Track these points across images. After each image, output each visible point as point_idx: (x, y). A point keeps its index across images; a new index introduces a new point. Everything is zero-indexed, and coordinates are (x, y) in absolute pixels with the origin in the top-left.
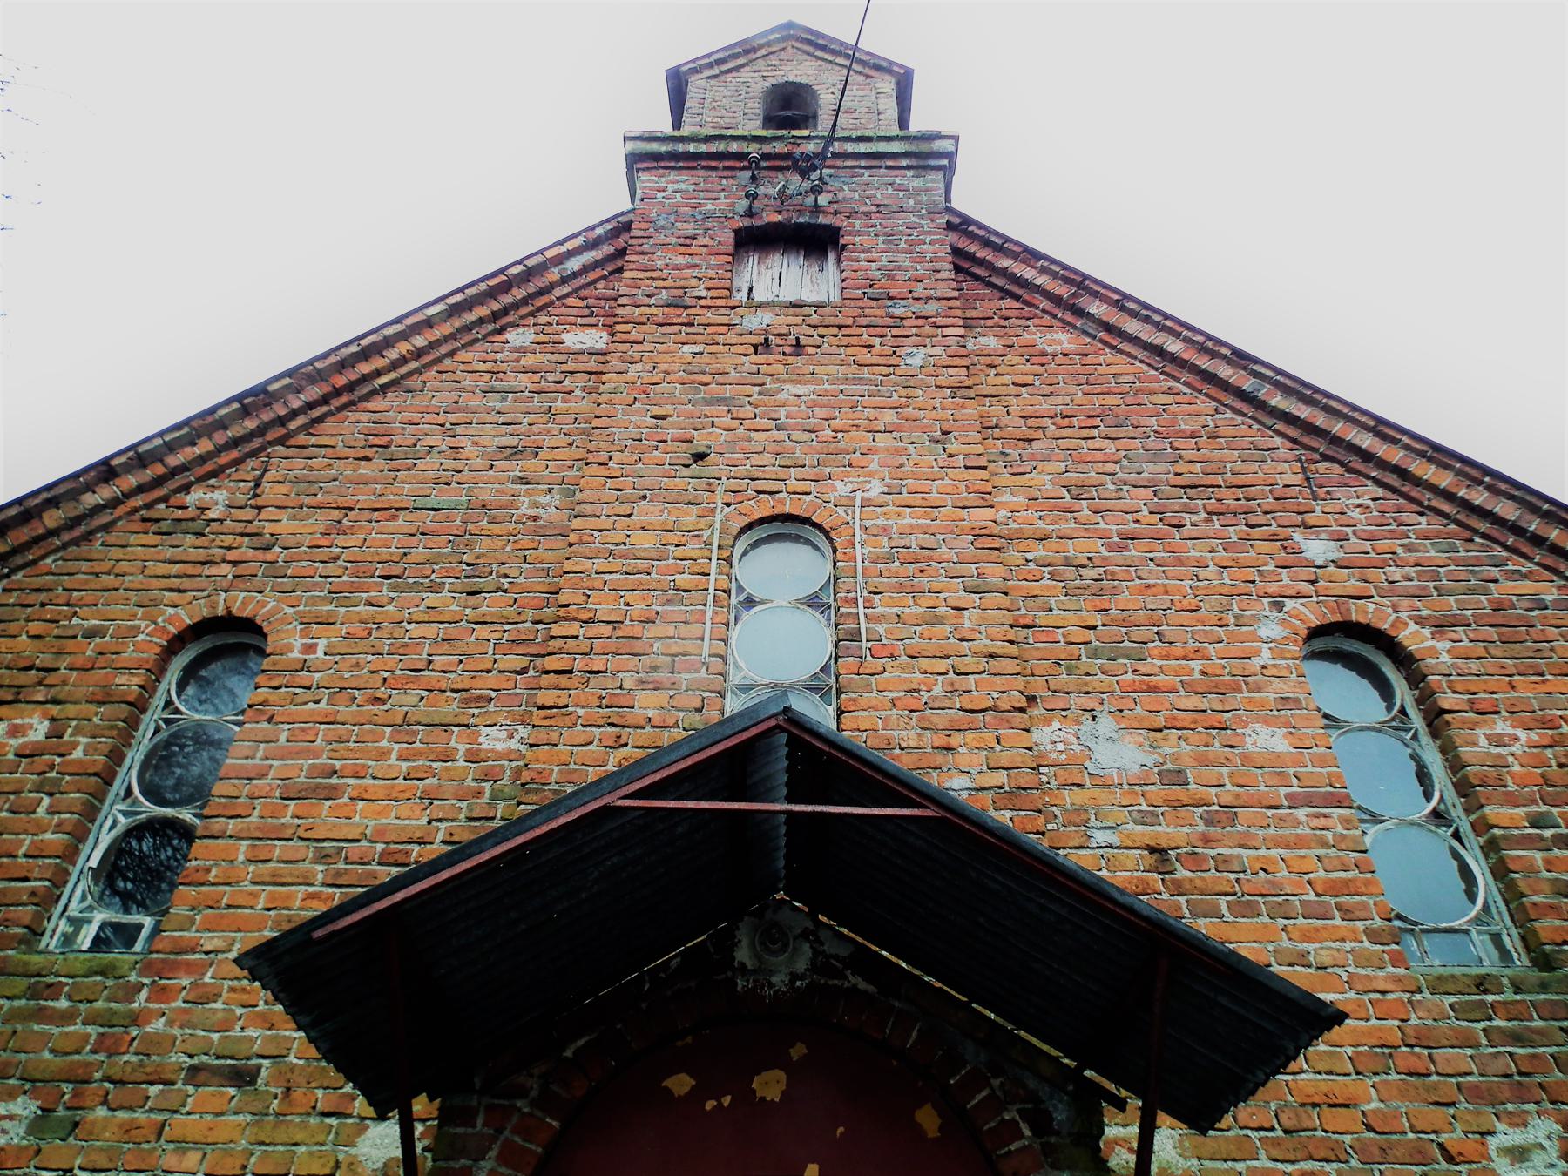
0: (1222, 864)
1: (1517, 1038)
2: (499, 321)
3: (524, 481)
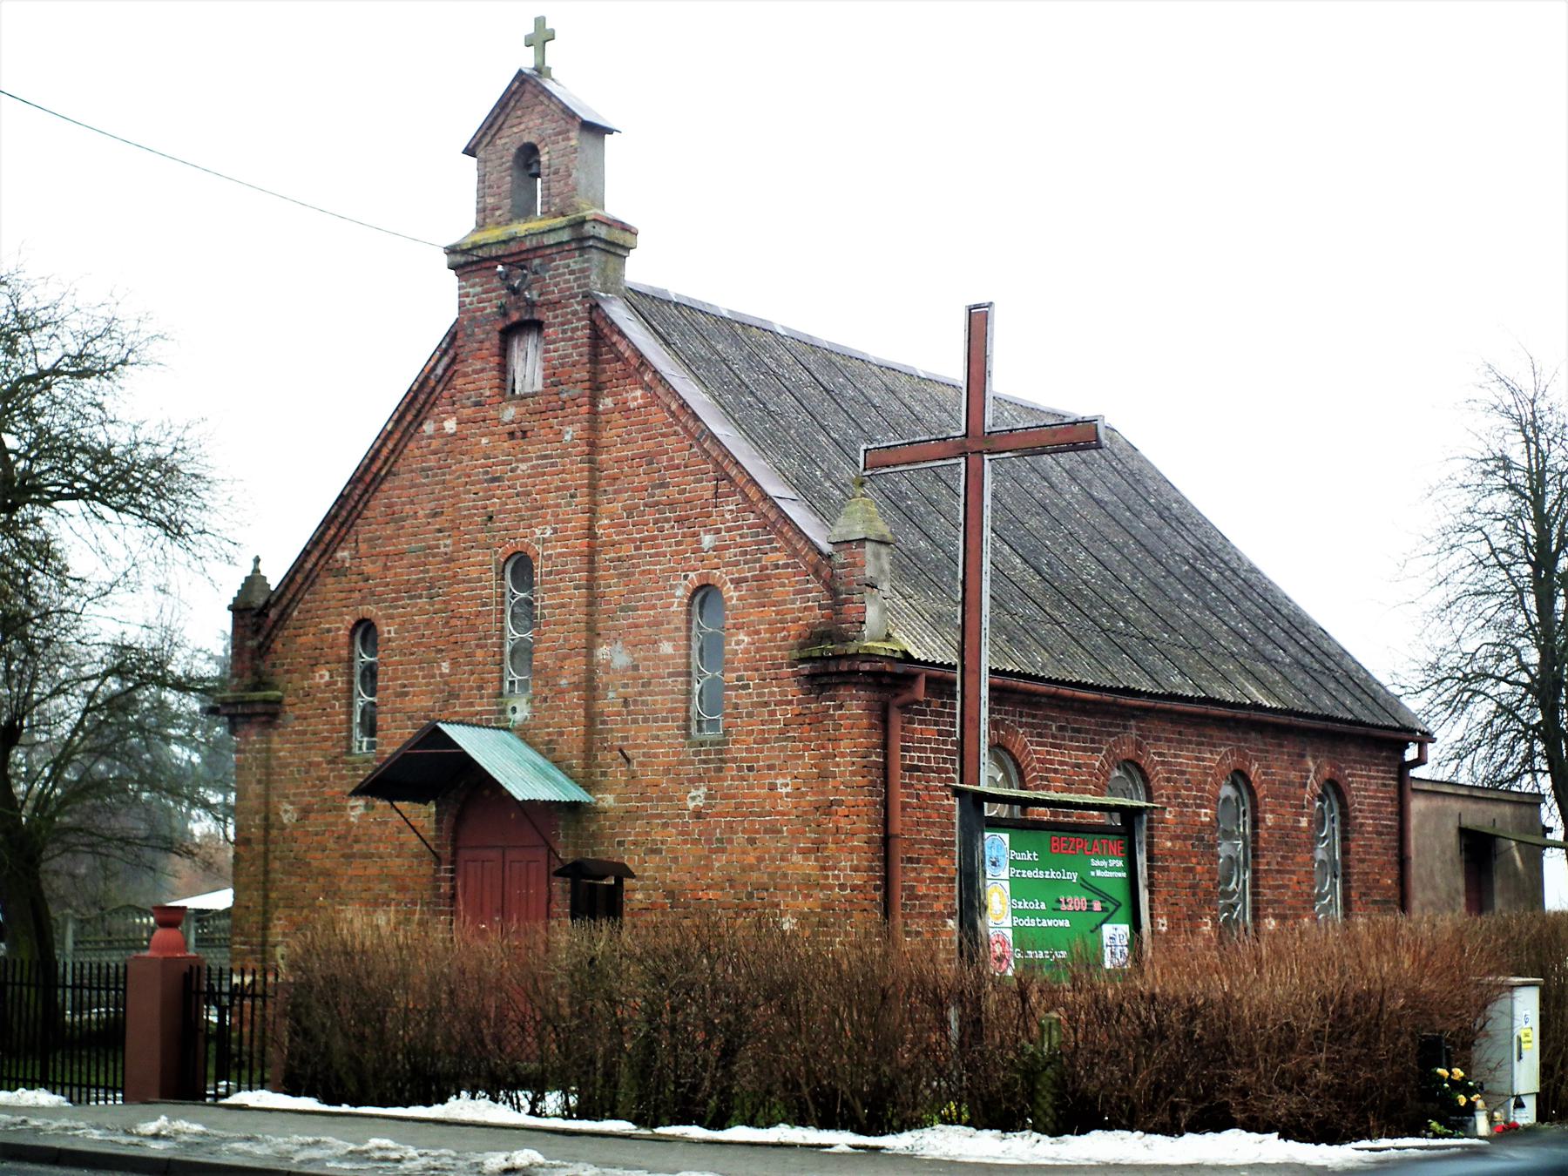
0: (644, 703)
1: (705, 762)
2: (419, 421)
3: (440, 531)
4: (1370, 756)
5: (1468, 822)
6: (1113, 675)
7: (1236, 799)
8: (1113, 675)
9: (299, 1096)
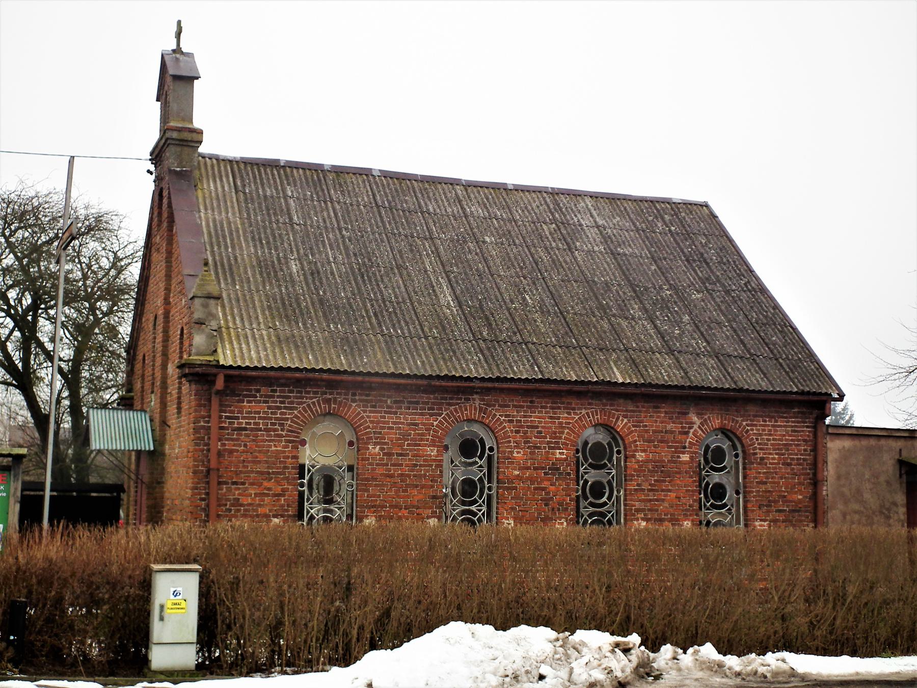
4: (776, 412)
5: (905, 455)
6: (686, 373)
7: (609, 444)
8: (686, 373)
9: (509, 629)
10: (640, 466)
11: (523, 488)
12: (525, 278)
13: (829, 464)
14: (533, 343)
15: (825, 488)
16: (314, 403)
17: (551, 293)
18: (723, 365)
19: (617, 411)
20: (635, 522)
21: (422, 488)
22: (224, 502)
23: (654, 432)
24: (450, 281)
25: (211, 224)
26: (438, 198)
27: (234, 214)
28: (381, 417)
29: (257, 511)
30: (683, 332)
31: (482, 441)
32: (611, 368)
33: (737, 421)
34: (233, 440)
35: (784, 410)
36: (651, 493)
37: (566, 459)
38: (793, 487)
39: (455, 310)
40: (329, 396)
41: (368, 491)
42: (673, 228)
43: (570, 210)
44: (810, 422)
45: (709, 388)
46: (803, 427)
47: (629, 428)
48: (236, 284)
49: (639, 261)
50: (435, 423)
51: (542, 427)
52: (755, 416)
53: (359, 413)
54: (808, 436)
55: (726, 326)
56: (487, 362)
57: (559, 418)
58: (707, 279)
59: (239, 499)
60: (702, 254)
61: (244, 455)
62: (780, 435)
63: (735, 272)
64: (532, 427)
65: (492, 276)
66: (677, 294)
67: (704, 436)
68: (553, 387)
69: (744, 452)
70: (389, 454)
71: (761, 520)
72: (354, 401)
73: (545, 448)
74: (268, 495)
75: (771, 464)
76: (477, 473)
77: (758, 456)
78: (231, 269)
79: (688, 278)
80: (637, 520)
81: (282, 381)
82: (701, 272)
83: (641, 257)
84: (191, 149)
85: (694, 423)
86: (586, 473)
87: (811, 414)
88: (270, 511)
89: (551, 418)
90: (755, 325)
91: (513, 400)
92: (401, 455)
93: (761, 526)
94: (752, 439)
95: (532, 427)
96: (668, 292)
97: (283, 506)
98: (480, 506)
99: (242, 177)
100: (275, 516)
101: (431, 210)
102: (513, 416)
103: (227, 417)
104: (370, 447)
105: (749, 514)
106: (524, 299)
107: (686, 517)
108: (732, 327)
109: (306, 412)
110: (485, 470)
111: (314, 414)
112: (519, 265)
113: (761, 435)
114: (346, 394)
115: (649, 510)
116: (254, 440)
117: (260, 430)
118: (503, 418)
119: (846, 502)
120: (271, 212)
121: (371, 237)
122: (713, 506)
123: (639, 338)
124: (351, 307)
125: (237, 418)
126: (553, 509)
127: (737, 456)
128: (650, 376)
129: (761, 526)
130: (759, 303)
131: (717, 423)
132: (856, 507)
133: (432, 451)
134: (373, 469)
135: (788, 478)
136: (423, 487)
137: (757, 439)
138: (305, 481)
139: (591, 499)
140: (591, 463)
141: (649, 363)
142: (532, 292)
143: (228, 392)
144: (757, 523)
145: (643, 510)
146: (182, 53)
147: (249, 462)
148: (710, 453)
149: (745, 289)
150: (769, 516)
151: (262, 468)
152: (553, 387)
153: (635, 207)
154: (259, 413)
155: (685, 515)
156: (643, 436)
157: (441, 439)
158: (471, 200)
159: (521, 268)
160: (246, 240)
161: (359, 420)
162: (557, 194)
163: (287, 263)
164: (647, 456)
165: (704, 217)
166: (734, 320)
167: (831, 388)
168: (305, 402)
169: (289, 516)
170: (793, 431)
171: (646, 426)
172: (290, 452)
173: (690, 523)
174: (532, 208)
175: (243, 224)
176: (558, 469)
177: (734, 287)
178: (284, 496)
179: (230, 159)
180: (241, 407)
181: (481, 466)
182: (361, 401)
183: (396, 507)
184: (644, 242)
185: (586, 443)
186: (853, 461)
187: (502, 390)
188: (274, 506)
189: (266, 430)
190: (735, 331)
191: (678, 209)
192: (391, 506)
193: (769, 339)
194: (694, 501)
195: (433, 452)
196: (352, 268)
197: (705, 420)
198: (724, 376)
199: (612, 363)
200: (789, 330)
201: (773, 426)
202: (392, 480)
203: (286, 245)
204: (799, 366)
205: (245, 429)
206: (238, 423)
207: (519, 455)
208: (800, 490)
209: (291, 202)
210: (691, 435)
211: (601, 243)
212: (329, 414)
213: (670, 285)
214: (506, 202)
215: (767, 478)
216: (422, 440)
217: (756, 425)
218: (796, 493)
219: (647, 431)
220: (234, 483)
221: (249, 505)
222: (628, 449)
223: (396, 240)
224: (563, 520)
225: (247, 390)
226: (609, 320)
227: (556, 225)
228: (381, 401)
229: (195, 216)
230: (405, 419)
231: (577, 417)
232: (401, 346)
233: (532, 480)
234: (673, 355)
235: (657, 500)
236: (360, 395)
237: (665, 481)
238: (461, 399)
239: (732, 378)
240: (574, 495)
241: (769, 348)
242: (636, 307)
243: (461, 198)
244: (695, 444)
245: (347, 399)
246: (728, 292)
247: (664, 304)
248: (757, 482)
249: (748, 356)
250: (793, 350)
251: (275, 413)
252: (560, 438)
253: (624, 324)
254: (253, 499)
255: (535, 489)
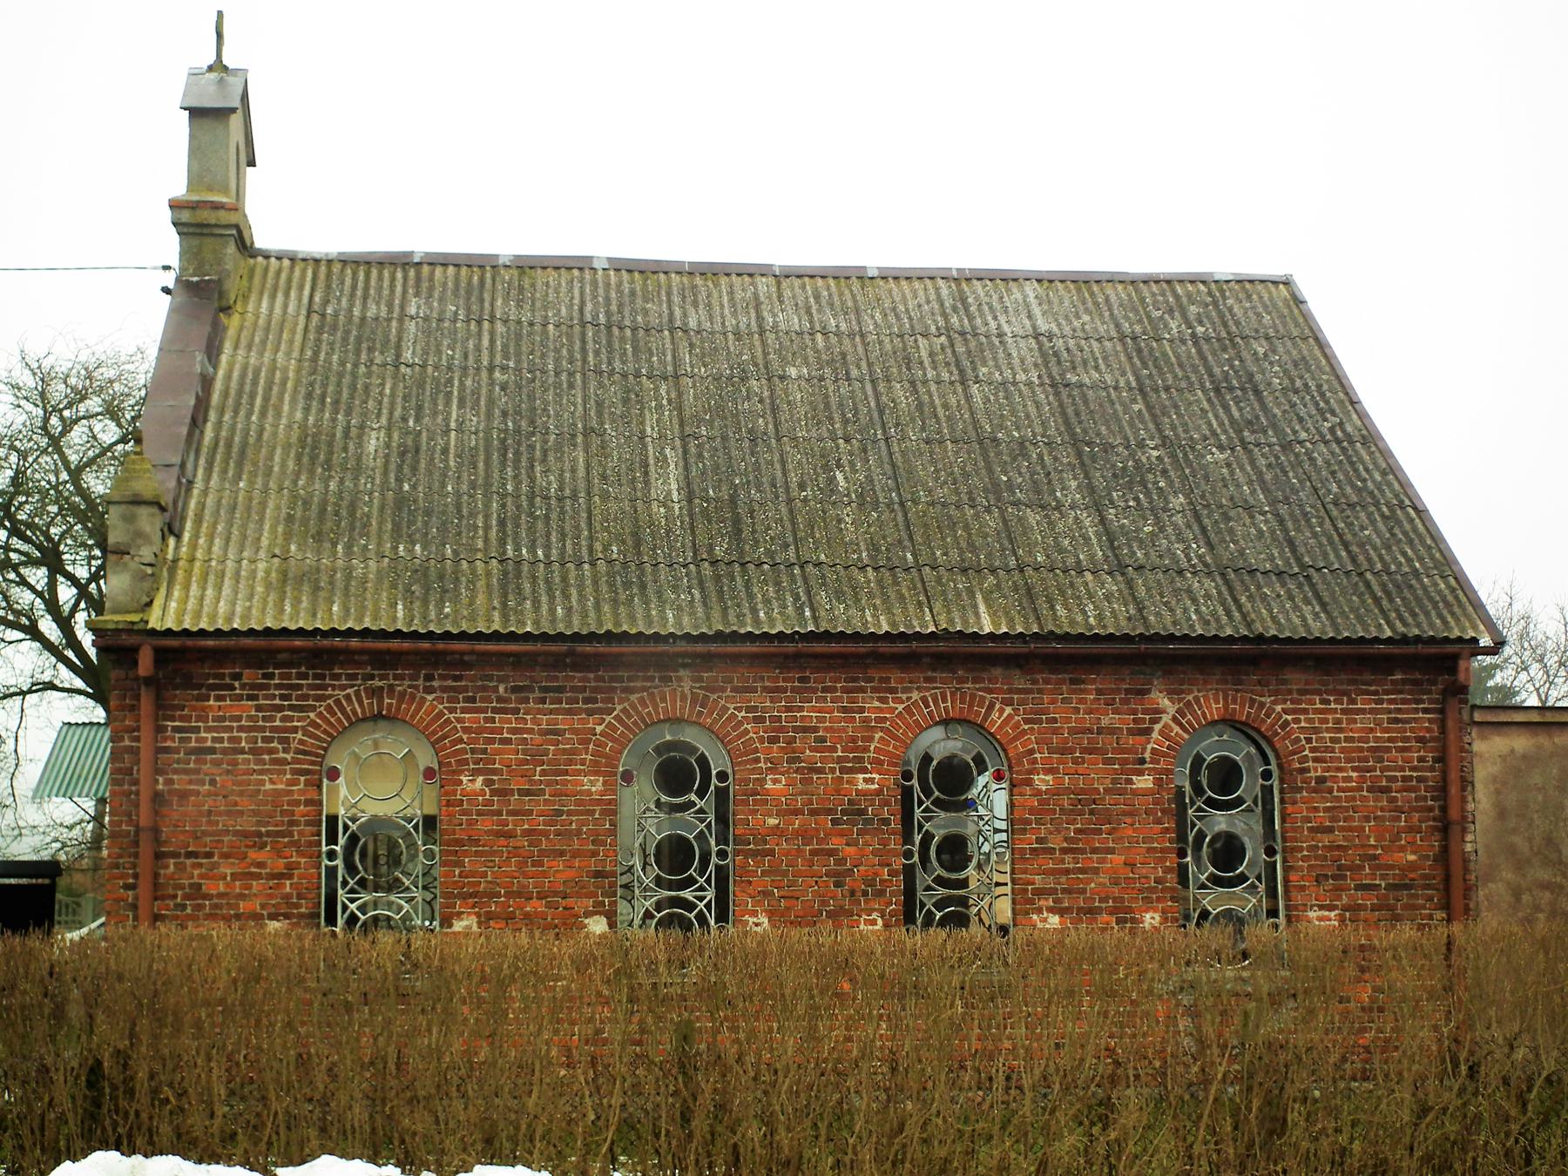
10: (1041, 802)
11: (788, 853)
12: (847, 441)
13: (1479, 786)
14: (819, 564)
15: (1469, 837)
16: (348, 697)
17: (893, 465)
18: (1231, 589)
19: (990, 691)
20: (1035, 917)
21: (574, 857)
22: (171, 891)
23: (1072, 731)
24: (685, 452)
25: (236, 374)
26: (715, 303)
27: (288, 354)
28: (487, 720)
29: (237, 907)
30: (1162, 530)
31: (703, 762)
32: (975, 607)
33: (1262, 705)
34: (186, 772)
35: (1368, 677)
36: (1068, 858)
37: (879, 792)
38: (1397, 838)
39: (677, 507)
40: (377, 683)
41: (460, 864)
42: (1200, 330)
43: (986, 308)
44: (1431, 701)
45: (1185, 638)
46: (1416, 711)
47: (1017, 725)
48: (240, 479)
49: (1109, 395)
50: (599, 729)
51: (826, 729)
52: (1302, 692)
53: (441, 714)
54: (1428, 730)
55: (1264, 513)
56: (705, 604)
57: (862, 710)
58: (1250, 423)
59: (200, 886)
60: (1251, 376)
61: (210, 800)
62: (1362, 730)
63: (1317, 404)
64: (805, 730)
65: (779, 440)
66: (1173, 456)
67: (1186, 736)
68: (834, 647)
69: (1280, 766)
70: (503, 793)
71: (1321, 908)
72: (429, 690)
73: (832, 770)
74: (258, 876)
75: (1340, 790)
76: (691, 826)
77: (1312, 774)
78: (242, 453)
79: (1209, 424)
80: (1039, 911)
81: (282, 657)
82: (1240, 409)
83: (1116, 388)
84: (220, 240)
85: (1164, 711)
86: (928, 819)
87: (1434, 683)
88: (263, 906)
89: (844, 710)
90: (1331, 507)
91: (762, 679)
92: (528, 793)
93: (1320, 919)
94: (1298, 740)
95: (805, 730)
96: (1155, 453)
97: (288, 896)
98: (701, 889)
99: (328, 286)
100: (273, 917)
101: (692, 323)
102: (764, 710)
103: (176, 729)
104: (465, 779)
105: (1293, 894)
106: (832, 480)
107: (1149, 904)
108: (1277, 516)
109: (333, 714)
110: (711, 817)
111: (348, 718)
112: (843, 415)
113: (1316, 731)
114: (414, 678)
115: (1064, 891)
116: (228, 772)
117: (242, 751)
118: (743, 714)
119: (1520, 865)
120: (364, 345)
121: (551, 380)
122: (1216, 881)
123: (1057, 544)
124: (459, 511)
125: (197, 730)
126: (852, 893)
127: (1267, 775)
128: (1055, 618)
129: (1320, 919)
130: (1352, 464)
131: (1215, 709)
132: (1544, 875)
133: (593, 783)
134: (471, 823)
135: (1383, 819)
136: (576, 854)
137: (1309, 740)
138: (338, 848)
139: (940, 872)
140: (938, 798)
141: (1063, 593)
142: (852, 464)
143: (178, 681)
144: (1312, 914)
145: (1053, 891)
146: (225, 68)
147: (220, 814)
148: (1204, 773)
149: (1328, 437)
150: (1339, 898)
151: (246, 824)
152: (834, 647)
153: (1129, 295)
154: (239, 719)
155: (1147, 900)
156: (1048, 742)
157: (612, 760)
158: (782, 302)
159: (846, 422)
160: (293, 401)
161: (442, 727)
162: (968, 280)
163: (360, 436)
164: (1059, 781)
165: (1274, 305)
166: (1286, 501)
167: (1475, 627)
168: (330, 696)
169: (301, 916)
170: (1391, 721)
171: (1055, 720)
172: (301, 792)
173: (1157, 917)
174: (907, 310)
175: (298, 371)
176: (862, 812)
177: (1303, 435)
178: (290, 877)
179: (318, 256)
180: (204, 709)
181: (701, 811)
182: (444, 689)
183: (519, 894)
184: (1130, 358)
185: (927, 759)
186: (1537, 779)
187: (736, 658)
188: (271, 896)
189: (253, 751)
190: (1281, 522)
191: (1222, 292)
192: (509, 895)
193: (1355, 535)
194: (1167, 870)
195: (594, 785)
196: (488, 440)
197: (1188, 704)
198: (1228, 613)
199: (979, 597)
200: (1408, 514)
201: (1344, 711)
202: (512, 842)
203: (371, 404)
204: (1411, 587)
205: (212, 751)
206: (197, 740)
207: (778, 786)
208: (1412, 843)
209: (411, 327)
210: (1155, 735)
211: (1036, 365)
212: (377, 717)
213: (1164, 438)
214: (855, 301)
215: (1333, 819)
216: (570, 762)
217: (1305, 711)
218: (1402, 849)
219: (1056, 731)
220: (189, 855)
221: (220, 895)
222: (1015, 769)
223: (600, 383)
224: (875, 915)
225: (216, 676)
226: (1002, 511)
227: (949, 337)
228: (484, 689)
229: (195, 358)
230: (536, 722)
231: (901, 707)
232: (534, 579)
233: (805, 835)
234: (1123, 574)
235: (1082, 871)
236: (443, 678)
237: (1099, 832)
238: (652, 679)
239: (1244, 616)
240: (899, 863)
241: (1349, 552)
242: (1074, 484)
243: (762, 299)
244: (1165, 755)
245: (416, 687)
246: (1286, 447)
247: (1136, 478)
248: (1311, 830)
249: (1296, 570)
250: (1404, 554)
251: (272, 719)
252: (866, 750)
253: (1032, 517)
254: (227, 885)
255: (814, 853)
